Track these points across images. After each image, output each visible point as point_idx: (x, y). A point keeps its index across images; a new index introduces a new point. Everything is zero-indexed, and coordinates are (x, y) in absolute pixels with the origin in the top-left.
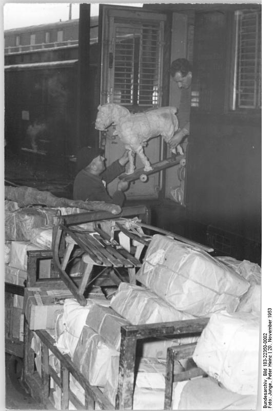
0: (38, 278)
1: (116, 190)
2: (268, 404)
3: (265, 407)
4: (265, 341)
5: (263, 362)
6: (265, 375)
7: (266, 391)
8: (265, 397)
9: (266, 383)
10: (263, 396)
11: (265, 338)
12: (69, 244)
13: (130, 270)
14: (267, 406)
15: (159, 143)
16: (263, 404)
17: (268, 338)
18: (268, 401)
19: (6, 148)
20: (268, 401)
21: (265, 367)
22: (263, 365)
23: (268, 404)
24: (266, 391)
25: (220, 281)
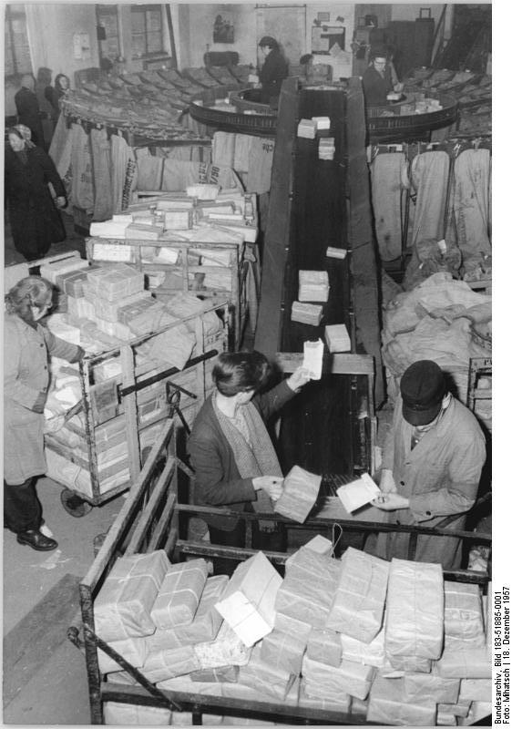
3: (498, 722)
6: (498, 665)
8: (498, 704)
9: (499, 680)
11: (498, 600)
14: (502, 720)
18: (503, 712)
20: (503, 712)
21: (498, 652)
22: (494, 647)
23: (503, 716)
24: (499, 693)
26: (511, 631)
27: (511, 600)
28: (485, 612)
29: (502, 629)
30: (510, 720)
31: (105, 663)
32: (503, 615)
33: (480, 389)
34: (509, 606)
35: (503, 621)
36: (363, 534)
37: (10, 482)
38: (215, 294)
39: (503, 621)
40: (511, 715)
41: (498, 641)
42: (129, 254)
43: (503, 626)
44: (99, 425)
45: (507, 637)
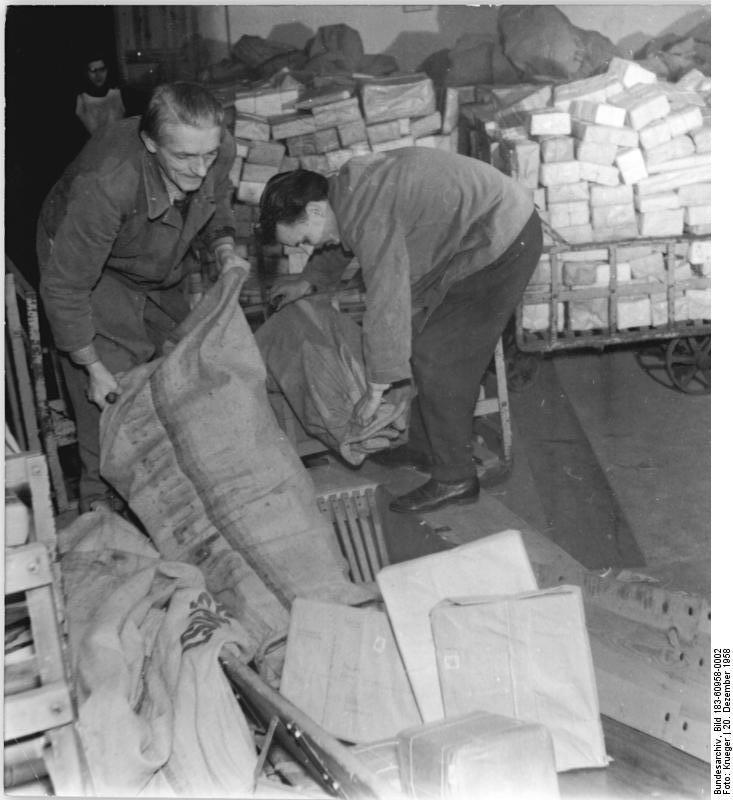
0: (336, 128)
1: (295, 591)
3: (717, 792)
4: (717, 664)
5: (713, 704)
7: (719, 761)
8: (718, 772)
10: (713, 771)
11: (717, 658)
12: (30, 643)
13: (273, 678)
14: (722, 790)
15: (339, 548)
16: (714, 787)
17: (723, 762)
18: (723, 781)
19: (6, 109)
20: (723, 781)
21: (718, 715)
22: (713, 710)
23: (723, 786)
24: (719, 761)
25: (240, 647)
26: (731, 697)
27: (731, 663)
30: (731, 791)
32: (723, 680)
34: (730, 670)
35: (723, 687)
40: (731, 785)
41: (718, 704)
45: (727, 704)
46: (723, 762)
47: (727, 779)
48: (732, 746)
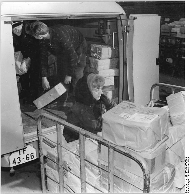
2: (188, 191)
3: (186, 192)
5: (185, 158)
7: (187, 185)
8: (186, 187)
11: (186, 160)
14: (187, 191)
17: (188, 185)
18: (188, 189)
20: (188, 189)
21: (186, 173)
23: (188, 191)
26: (189, 169)
27: (189, 161)
28: (131, 157)
29: (187, 169)
30: (189, 192)
31: (79, 159)
32: (188, 165)
33: (112, 76)
34: (189, 162)
35: (188, 166)
36: (19, 151)
37: (3, 166)
38: (59, 144)
39: (188, 166)
40: (189, 190)
42: (10, 19)
43: (188, 168)
44: (103, 69)
46: (188, 185)
47: (189, 189)
48: (189, 181)
